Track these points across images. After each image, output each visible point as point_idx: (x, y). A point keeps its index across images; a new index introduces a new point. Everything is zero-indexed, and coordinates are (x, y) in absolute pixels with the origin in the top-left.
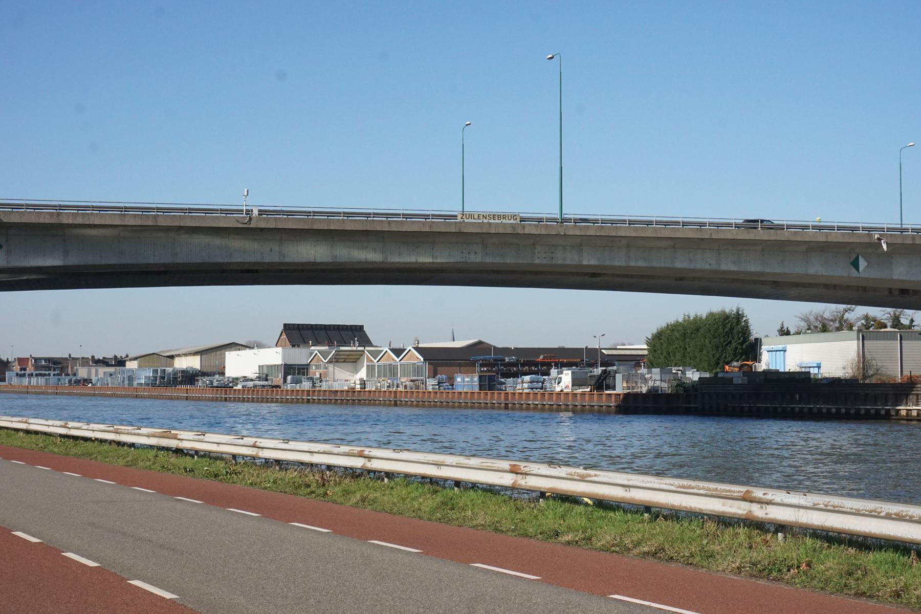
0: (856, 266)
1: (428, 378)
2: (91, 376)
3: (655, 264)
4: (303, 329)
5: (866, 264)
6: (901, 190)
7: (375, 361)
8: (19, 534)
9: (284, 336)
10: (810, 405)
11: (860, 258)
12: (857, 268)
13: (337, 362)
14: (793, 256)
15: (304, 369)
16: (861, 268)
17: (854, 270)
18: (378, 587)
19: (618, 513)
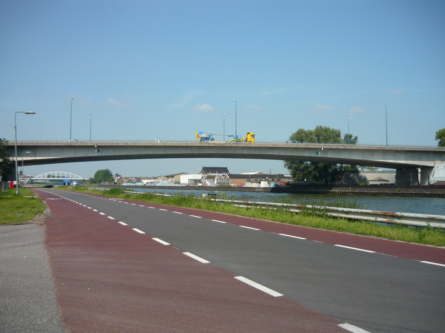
0: (318, 154)
1: (438, 168)
2: (180, 180)
3: (168, 153)
4: (217, 169)
5: (320, 153)
6: (387, 132)
7: (224, 178)
8: (136, 230)
9: (203, 171)
10: (428, 192)
11: (319, 152)
12: (318, 154)
13: (208, 178)
14: (212, 151)
15: (200, 180)
16: (319, 154)
17: (317, 155)
18: (88, 314)
19: (383, 229)
